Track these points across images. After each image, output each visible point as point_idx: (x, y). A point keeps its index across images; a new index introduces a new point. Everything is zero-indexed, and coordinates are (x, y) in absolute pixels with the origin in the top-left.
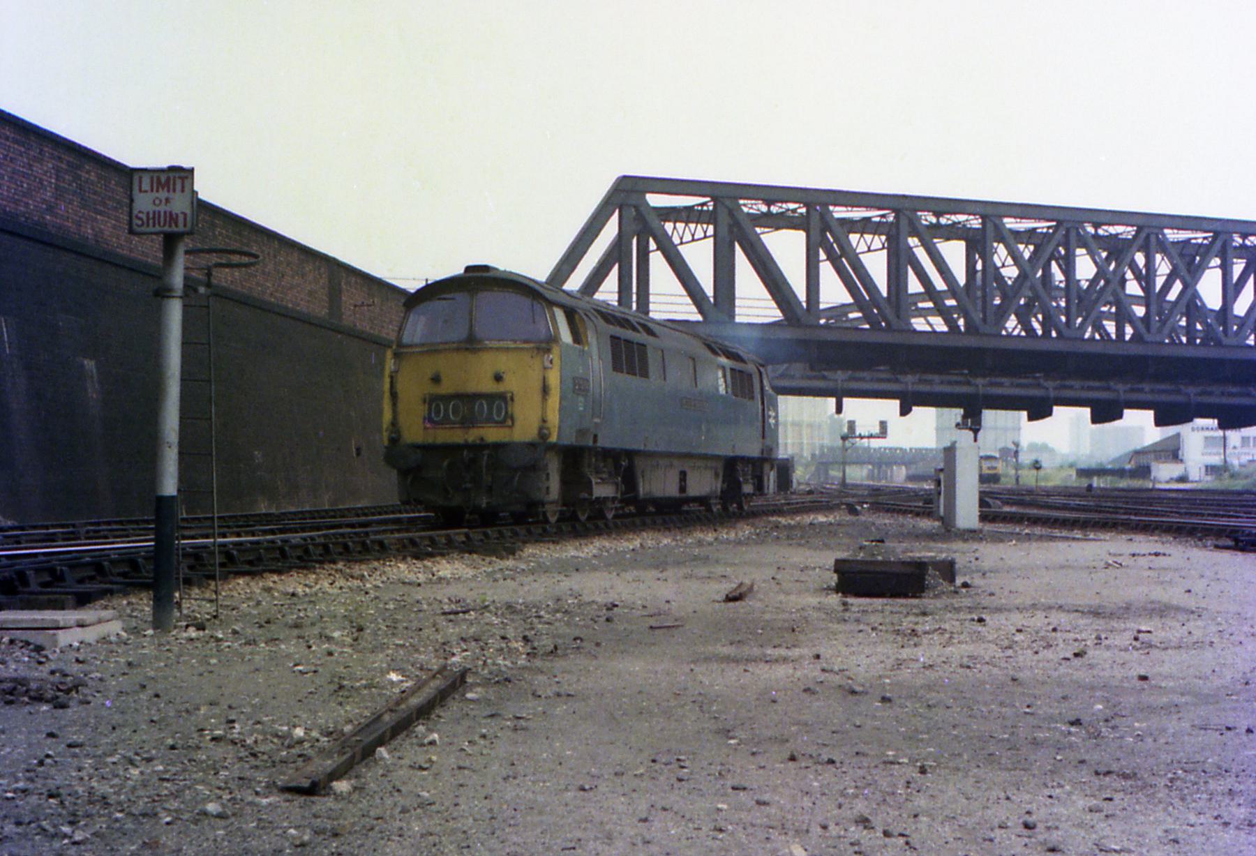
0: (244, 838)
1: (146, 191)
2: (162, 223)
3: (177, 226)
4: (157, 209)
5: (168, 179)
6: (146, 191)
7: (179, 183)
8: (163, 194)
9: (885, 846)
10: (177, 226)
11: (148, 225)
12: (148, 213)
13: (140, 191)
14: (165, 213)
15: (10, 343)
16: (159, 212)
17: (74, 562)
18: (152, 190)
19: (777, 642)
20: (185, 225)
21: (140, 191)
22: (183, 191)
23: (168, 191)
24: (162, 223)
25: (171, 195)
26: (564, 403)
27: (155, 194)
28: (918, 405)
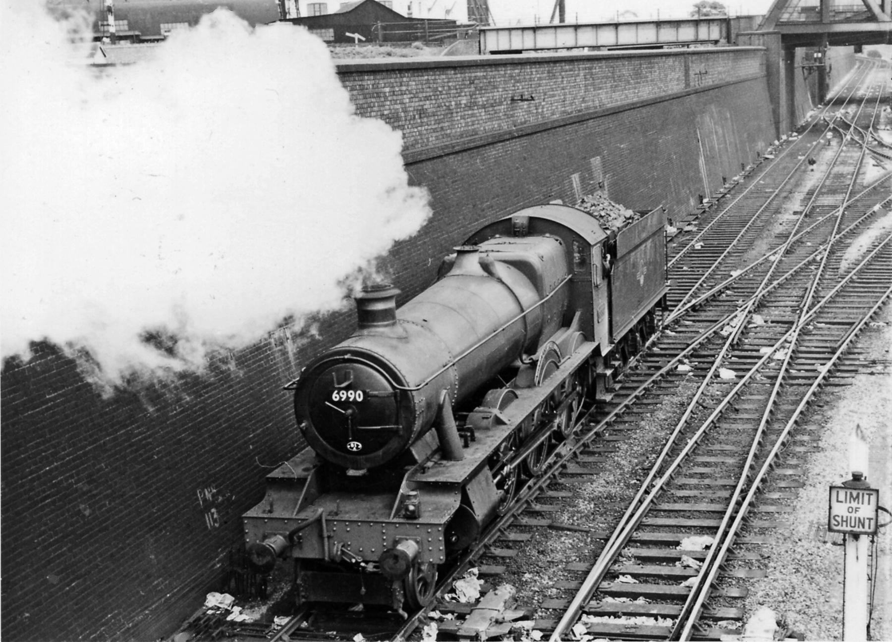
0: (622, 488)
1: (841, 502)
2: (853, 525)
3: (863, 527)
4: (849, 515)
5: (858, 494)
6: (841, 502)
7: (866, 497)
8: (854, 505)
9: (220, 603)
10: (863, 527)
11: (842, 526)
12: (842, 517)
13: (838, 501)
14: (855, 518)
15: (746, 267)
16: (851, 518)
17: (702, 420)
18: (846, 502)
19: (695, 141)
20: (869, 528)
21: (838, 501)
22: (869, 504)
23: (858, 503)
24: (853, 525)
25: (860, 505)
26: (426, 22)
27: (848, 505)
28: (431, 221)
